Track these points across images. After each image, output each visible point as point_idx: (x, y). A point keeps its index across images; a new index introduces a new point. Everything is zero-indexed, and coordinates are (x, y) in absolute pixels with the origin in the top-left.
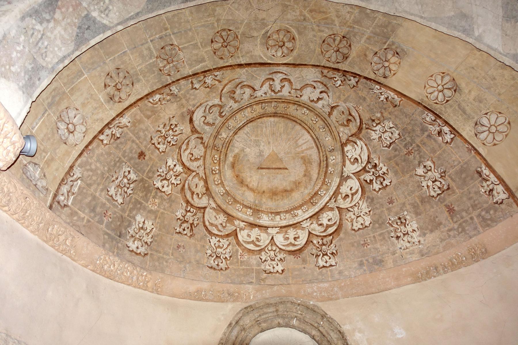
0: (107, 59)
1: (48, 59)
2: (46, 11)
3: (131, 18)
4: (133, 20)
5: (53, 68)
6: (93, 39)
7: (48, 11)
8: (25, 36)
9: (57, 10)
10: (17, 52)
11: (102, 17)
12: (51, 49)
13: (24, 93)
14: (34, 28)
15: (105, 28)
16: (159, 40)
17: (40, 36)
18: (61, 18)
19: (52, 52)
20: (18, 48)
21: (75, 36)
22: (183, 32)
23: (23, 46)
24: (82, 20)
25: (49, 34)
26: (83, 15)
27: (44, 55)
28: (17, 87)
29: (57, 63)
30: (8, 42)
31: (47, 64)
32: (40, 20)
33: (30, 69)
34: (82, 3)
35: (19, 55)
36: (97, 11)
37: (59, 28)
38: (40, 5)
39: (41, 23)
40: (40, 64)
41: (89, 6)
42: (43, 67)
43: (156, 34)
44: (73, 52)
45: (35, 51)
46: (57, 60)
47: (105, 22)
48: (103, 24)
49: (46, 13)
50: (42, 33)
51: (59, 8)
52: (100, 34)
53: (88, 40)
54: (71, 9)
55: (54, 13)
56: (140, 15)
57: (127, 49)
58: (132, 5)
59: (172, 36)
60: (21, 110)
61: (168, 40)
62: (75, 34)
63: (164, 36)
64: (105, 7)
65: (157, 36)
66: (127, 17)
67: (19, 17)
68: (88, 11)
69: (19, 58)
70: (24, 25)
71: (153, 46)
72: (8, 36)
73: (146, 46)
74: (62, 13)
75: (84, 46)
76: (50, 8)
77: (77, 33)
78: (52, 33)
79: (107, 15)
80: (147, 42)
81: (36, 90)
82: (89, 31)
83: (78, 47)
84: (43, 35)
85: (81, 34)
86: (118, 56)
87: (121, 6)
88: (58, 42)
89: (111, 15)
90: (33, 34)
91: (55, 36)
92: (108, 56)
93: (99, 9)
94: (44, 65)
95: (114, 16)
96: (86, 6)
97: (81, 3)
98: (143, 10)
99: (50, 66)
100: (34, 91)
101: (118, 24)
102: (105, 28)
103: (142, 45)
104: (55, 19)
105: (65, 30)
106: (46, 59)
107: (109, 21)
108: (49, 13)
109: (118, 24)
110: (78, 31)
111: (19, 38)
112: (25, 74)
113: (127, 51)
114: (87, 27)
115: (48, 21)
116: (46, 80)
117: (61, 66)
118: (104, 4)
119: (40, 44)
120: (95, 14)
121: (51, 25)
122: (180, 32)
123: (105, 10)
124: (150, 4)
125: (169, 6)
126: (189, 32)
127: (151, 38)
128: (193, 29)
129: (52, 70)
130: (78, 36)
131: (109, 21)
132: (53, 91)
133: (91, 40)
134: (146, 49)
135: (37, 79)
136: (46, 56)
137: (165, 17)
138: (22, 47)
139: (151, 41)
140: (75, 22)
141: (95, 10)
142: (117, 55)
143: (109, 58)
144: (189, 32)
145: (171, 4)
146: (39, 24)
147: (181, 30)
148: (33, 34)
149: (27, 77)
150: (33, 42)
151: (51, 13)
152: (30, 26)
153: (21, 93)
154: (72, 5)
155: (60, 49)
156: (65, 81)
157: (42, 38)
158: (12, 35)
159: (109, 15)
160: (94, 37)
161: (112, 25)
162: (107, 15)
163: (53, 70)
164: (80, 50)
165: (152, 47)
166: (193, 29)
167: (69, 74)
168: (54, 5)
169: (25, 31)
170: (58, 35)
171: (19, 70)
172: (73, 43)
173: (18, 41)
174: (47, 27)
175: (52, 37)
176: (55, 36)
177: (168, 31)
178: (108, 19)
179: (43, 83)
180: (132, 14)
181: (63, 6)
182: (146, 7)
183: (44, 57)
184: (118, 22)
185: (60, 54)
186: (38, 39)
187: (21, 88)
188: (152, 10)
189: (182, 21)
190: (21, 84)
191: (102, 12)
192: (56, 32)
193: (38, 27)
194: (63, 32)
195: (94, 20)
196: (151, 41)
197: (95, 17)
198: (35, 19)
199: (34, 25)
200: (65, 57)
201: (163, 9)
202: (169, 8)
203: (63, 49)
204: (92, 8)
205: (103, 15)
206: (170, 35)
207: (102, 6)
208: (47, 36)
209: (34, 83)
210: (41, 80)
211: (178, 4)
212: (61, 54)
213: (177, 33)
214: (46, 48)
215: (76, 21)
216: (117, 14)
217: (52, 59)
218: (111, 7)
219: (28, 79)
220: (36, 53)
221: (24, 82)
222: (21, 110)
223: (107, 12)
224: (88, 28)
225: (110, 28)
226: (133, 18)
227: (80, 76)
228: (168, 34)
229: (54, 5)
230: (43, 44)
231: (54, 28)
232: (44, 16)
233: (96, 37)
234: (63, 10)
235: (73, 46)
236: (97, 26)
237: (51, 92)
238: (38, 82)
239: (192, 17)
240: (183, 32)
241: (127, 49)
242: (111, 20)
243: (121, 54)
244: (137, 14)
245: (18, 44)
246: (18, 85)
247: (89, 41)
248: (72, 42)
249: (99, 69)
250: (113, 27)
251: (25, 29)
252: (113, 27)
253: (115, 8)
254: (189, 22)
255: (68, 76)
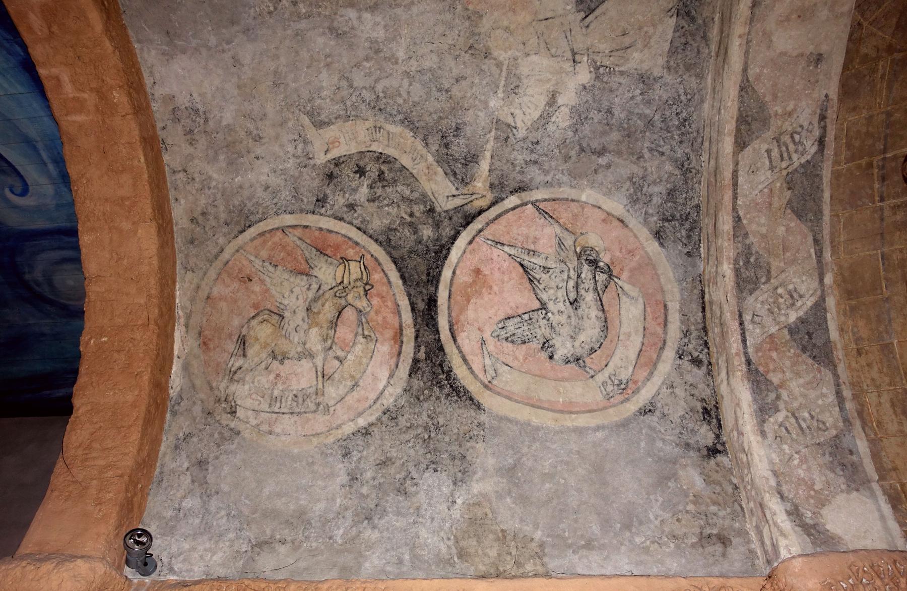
0: (882, 294)
1: (830, 421)
2: (764, 395)
3: (819, 254)
4: (824, 253)
5: (847, 421)
6: (830, 332)
7: (766, 392)
8: (786, 443)
9: (768, 377)
10: (799, 466)
11: (801, 306)
12: (818, 410)
13: (857, 490)
14: (779, 423)
15: (820, 306)
16: (885, 183)
17: (793, 420)
18: (780, 376)
19: (822, 412)
20: (796, 462)
21: (814, 363)
22: (888, 131)
23: (796, 453)
24: (795, 340)
25: (796, 404)
26: (788, 337)
27: (821, 426)
28: (845, 495)
29: (842, 409)
30: (782, 473)
31: (836, 427)
32: (773, 410)
33: (831, 459)
34: (770, 333)
35: (804, 466)
36: (789, 311)
37: (793, 385)
38: (755, 400)
39: (777, 410)
40: (831, 438)
41: (778, 323)
42: (836, 436)
43: (872, 188)
44: (836, 376)
45: (810, 437)
46: (837, 409)
47: (809, 304)
48: (811, 307)
49: (767, 395)
50: (790, 415)
51: (768, 372)
52: (825, 318)
53: (828, 341)
54: (774, 355)
55: (771, 383)
56: (819, 237)
57: (879, 251)
58: (799, 249)
59: (888, 155)
60: (879, 510)
61: (893, 164)
62: (810, 361)
63: (881, 172)
64: (788, 296)
65: (877, 186)
66: (815, 261)
67: (759, 438)
68: (785, 327)
69: (809, 469)
70: (770, 436)
71: (894, 198)
72: (776, 468)
73: (887, 213)
74: (774, 371)
75: (835, 353)
76: (763, 387)
77: (810, 356)
78: (796, 399)
79: (801, 296)
80: (882, 209)
81: (863, 467)
82: (814, 335)
83: (832, 365)
84: (793, 414)
85: (814, 350)
86: (884, 271)
87: (795, 269)
88: (812, 394)
89: (803, 289)
90: (786, 429)
91: (801, 395)
92: (877, 289)
93: (788, 308)
94: (834, 432)
95: (805, 283)
96: (777, 327)
97: (770, 335)
98: (812, 231)
99: (841, 424)
100: (864, 472)
101: (821, 280)
102: (819, 307)
103: (882, 220)
104: (778, 385)
105: (798, 375)
106: (828, 425)
107: (812, 295)
108: (768, 390)
109: (821, 280)
110: (808, 353)
111: (785, 454)
112: (834, 472)
113: (881, 252)
114: (807, 337)
115: (778, 397)
116: (858, 442)
117: (849, 405)
118: (782, 297)
119: (804, 425)
120: (793, 317)
121: (784, 394)
122: (886, 137)
123: (792, 297)
124: (806, 215)
125: (821, 179)
126: (892, 119)
127: (877, 198)
128: (889, 108)
129: (847, 424)
130: (814, 357)
131: (812, 295)
132: (894, 410)
133: (829, 337)
134: (895, 214)
135: (849, 456)
136: (824, 423)
137: (845, 164)
138: (797, 456)
139: (882, 199)
140: (794, 353)
141: (787, 315)
142: (882, 273)
143: (881, 288)
144: (892, 119)
145: (818, 175)
146: (778, 414)
147: (883, 135)
148: (786, 429)
149: (838, 470)
150: (798, 435)
151: (770, 388)
152: (776, 427)
153: (855, 493)
154: (769, 350)
155: (823, 395)
156: (887, 379)
157: (796, 418)
158: (777, 461)
159: (802, 293)
160: (827, 330)
161: (819, 293)
162: (801, 296)
163: (849, 421)
164: (837, 361)
165: (894, 201)
166: (889, 108)
167: (879, 369)
168: (762, 378)
169: (778, 439)
170: (802, 389)
171: (824, 478)
172: (822, 368)
173: (787, 457)
174: (786, 402)
175: (801, 400)
176: (801, 395)
177: (875, 163)
178: (807, 296)
179: (860, 450)
180: (812, 251)
181: (767, 365)
182: (810, 224)
183: (824, 428)
184: (818, 280)
185: (830, 400)
186: (796, 425)
187: (849, 490)
188: (819, 213)
189: (864, 130)
190: (843, 487)
191: (793, 304)
192: (797, 391)
193: (780, 416)
194: (801, 381)
195: (802, 321)
196: (882, 199)
197: (797, 319)
198: (770, 417)
199: (776, 422)
200: (838, 394)
201: (822, 191)
202: (824, 178)
203: (825, 390)
204: (783, 319)
205: (799, 304)
206: (884, 159)
207: (785, 300)
208: (798, 409)
209: (853, 464)
210: (854, 450)
211: (822, 162)
212: (831, 398)
213: (885, 145)
214: (812, 417)
215: (792, 351)
216: (804, 278)
217: (832, 415)
218: (791, 287)
219: (843, 470)
220: (813, 436)
221: (842, 480)
222: (879, 510)
223: (795, 295)
224: (809, 334)
225: (823, 299)
226: (821, 251)
227: (892, 352)
228: (880, 164)
229: (762, 378)
230: (804, 420)
231: (791, 394)
232: (769, 401)
233: (827, 327)
234: (771, 367)
235: (827, 371)
236: (811, 320)
237: (895, 413)
238: (854, 458)
239: (864, 108)
240: (888, 131)
241: (879, 251)
242: (811, 292)
243: (883, 264)
244: (816, 241)
245: (791, 458)
246: (842, 491)
247: (830, 341)
248: (820, 372)
249: (893, 314)
250: (823, 291)
251: (776, 437)
252: (823, 291)
253: (794, 280)
254: (871, 117)
255: (881, 372)
